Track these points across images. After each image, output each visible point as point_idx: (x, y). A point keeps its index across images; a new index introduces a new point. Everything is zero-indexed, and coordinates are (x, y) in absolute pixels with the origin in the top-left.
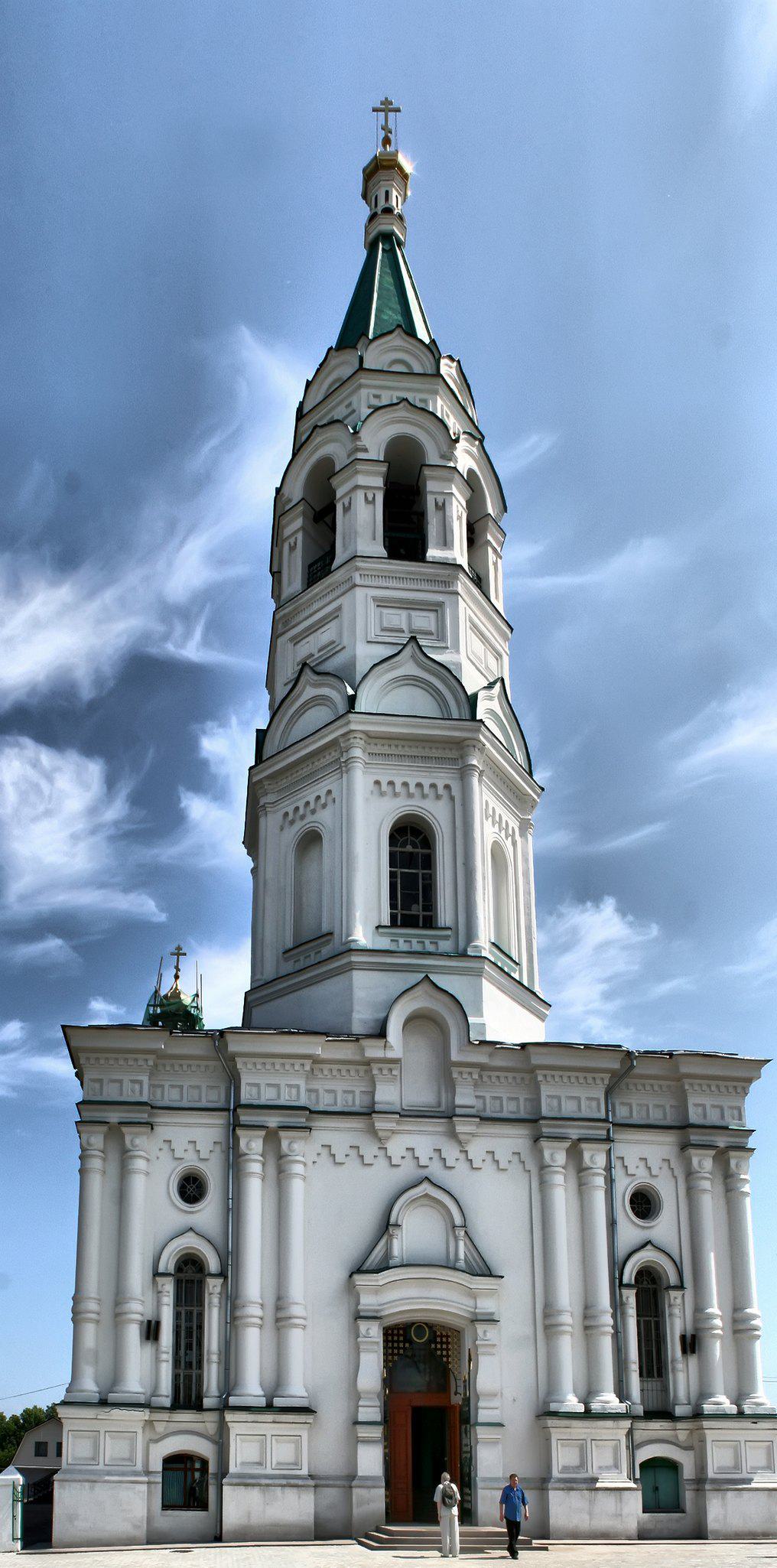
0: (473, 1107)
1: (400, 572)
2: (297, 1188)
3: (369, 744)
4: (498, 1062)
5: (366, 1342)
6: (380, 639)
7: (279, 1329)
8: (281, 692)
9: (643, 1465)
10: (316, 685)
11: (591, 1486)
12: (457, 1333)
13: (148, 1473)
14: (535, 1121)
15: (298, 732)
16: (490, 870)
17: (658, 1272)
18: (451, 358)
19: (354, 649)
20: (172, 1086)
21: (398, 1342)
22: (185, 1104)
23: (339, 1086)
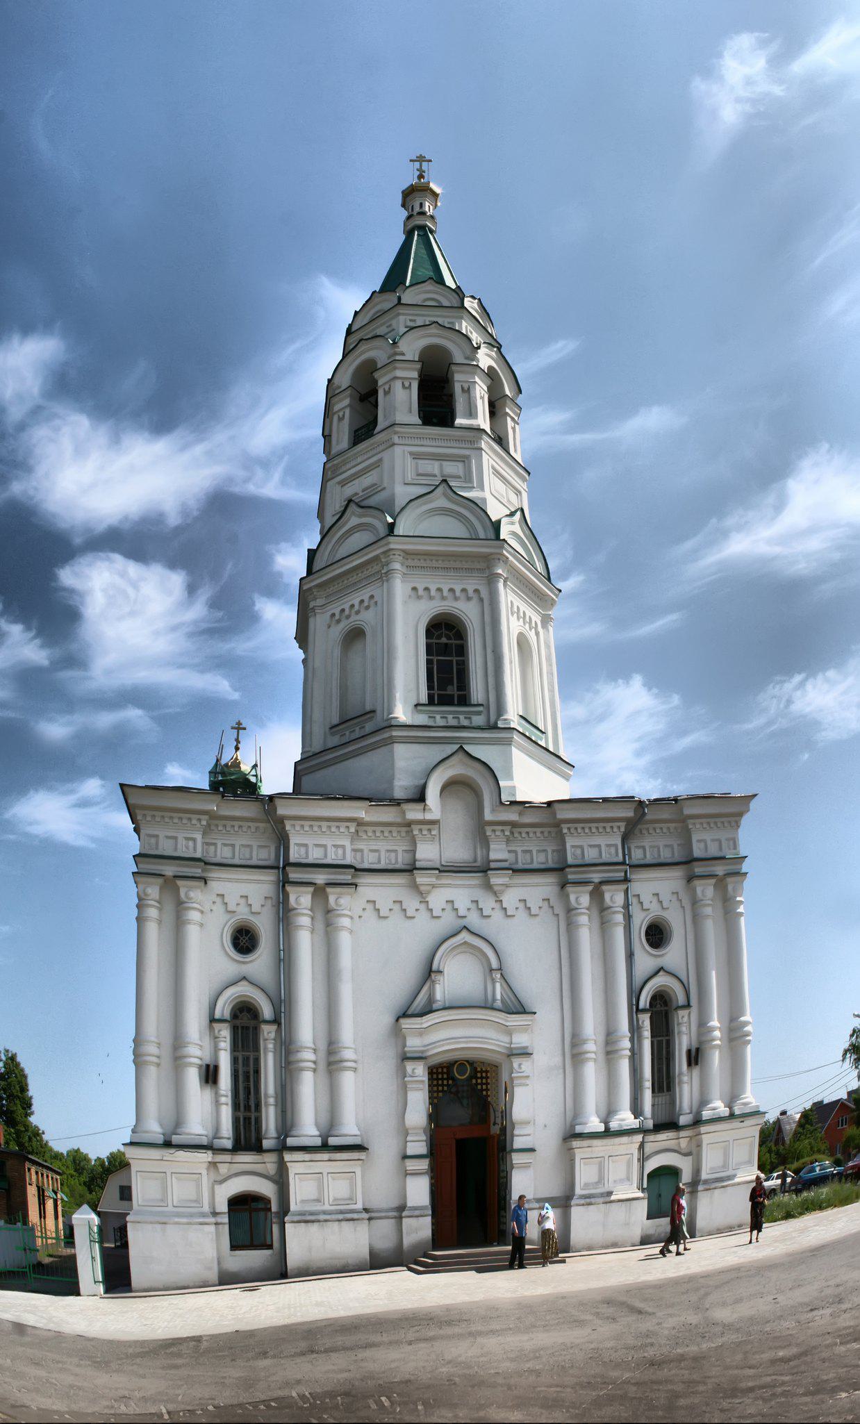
0: (506, 861)
1: (435, 435)
2: (345, 941)
3: (407, 559)
4: (528, 819)
5: (412, 1081)
6: (415, 482)
7: (331, 1072)
8: (329, 521)
9: (651, 1175)
10: (360, 516)
11: (607, 1199)
12: (496, 1067)
13: (215, 1214)
14: (562, 869)
15: (343, 551)
16: (518, 670)
17: (669, 995)
18: (473, 297)
19: (393, 489)
20: (225, 845)
21: (443, 1079)
22: (237, 861)
23: (382, 846)
